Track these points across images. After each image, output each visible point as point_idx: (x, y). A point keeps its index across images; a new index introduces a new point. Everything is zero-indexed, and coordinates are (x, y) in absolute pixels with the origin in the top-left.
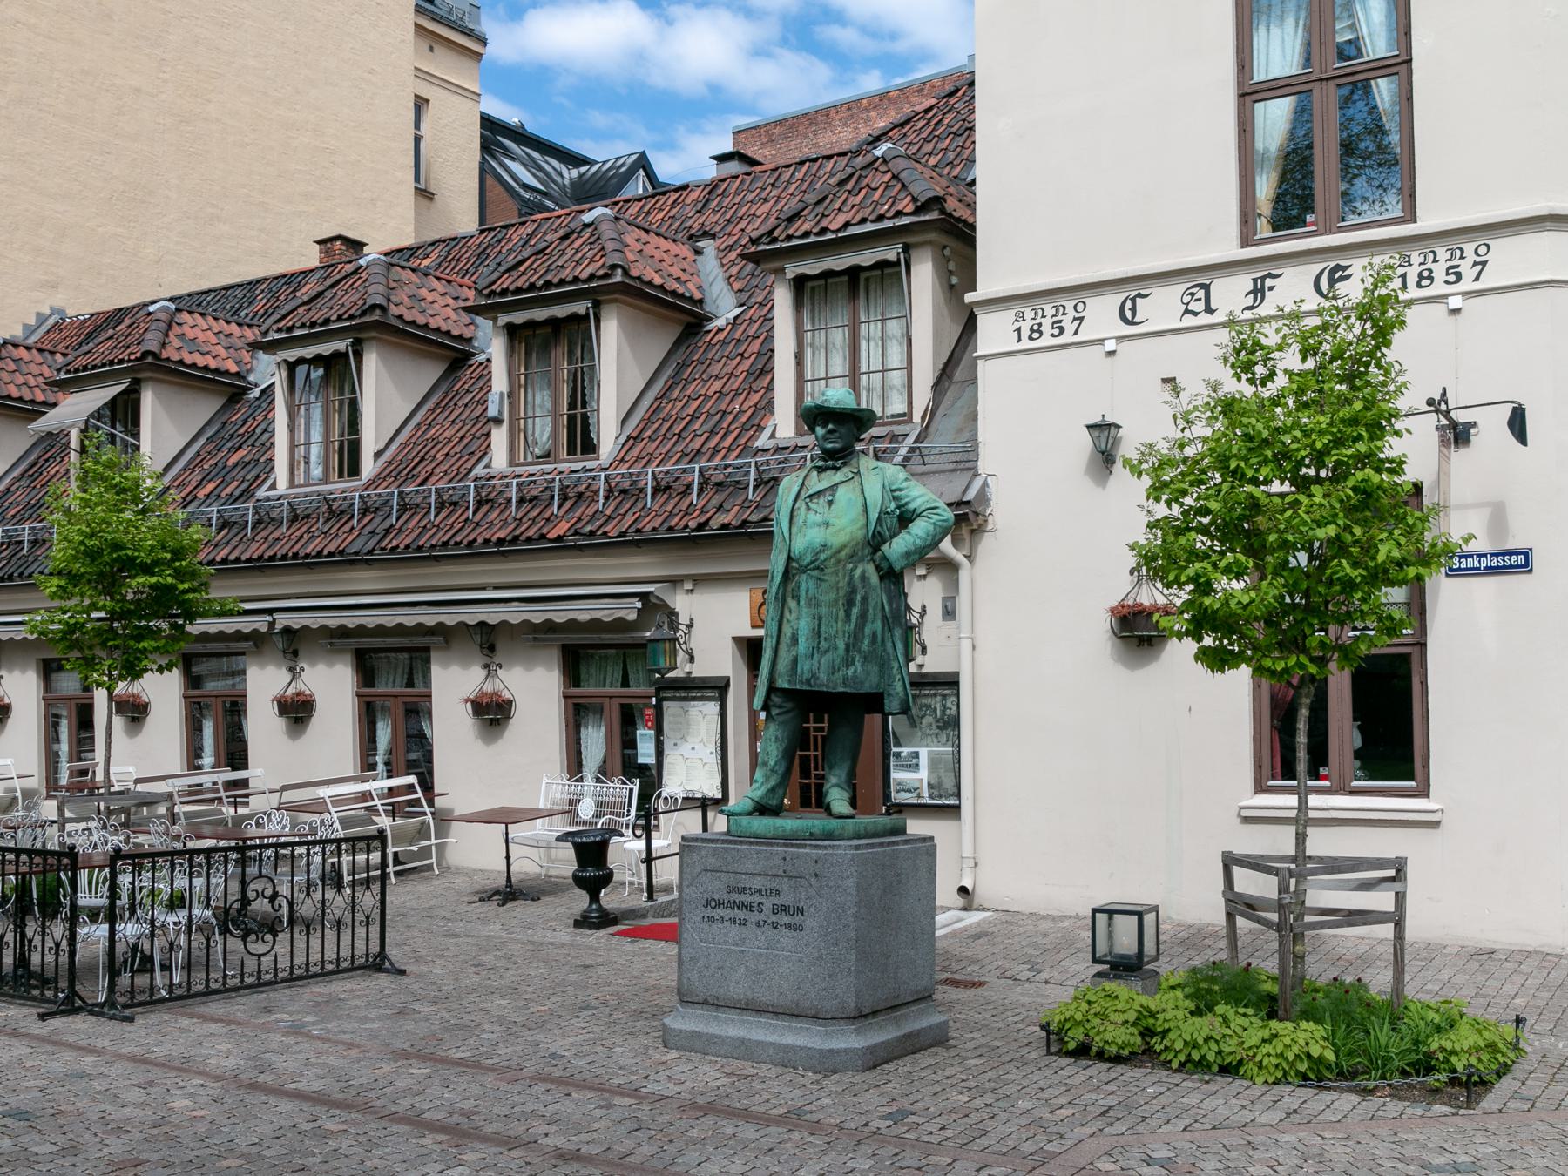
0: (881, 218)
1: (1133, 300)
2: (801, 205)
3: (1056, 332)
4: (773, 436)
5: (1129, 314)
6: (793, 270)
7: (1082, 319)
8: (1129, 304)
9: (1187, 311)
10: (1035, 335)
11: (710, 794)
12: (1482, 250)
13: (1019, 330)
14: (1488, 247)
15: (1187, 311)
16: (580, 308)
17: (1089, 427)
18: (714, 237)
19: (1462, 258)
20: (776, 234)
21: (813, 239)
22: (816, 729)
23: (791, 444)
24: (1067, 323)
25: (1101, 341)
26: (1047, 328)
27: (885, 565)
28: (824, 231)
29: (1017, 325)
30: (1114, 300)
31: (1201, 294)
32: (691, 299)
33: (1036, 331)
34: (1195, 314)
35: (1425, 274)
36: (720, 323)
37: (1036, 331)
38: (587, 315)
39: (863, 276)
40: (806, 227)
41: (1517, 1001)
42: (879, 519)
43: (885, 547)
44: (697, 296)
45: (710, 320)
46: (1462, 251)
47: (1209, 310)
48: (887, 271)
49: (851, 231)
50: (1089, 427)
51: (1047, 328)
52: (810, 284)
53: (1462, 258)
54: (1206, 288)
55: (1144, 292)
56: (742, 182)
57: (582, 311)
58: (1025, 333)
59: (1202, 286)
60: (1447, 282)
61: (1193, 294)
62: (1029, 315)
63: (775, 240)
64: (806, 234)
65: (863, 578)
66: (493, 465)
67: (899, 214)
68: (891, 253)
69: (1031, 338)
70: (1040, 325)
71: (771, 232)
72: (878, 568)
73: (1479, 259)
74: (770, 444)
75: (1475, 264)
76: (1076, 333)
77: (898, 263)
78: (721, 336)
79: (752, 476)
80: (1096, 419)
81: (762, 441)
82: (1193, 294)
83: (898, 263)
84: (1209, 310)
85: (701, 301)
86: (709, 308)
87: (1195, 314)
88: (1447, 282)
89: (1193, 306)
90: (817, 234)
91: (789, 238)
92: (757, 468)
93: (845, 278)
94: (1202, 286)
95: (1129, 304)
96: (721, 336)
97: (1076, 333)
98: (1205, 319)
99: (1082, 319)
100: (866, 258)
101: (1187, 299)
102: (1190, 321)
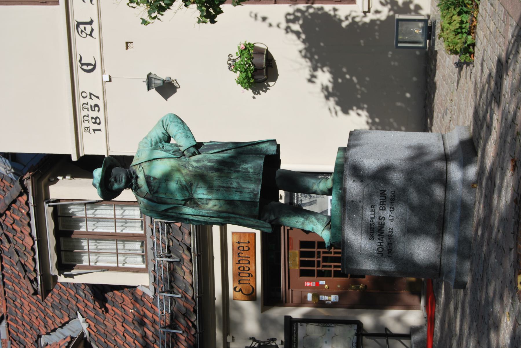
0: (29, 214)
1: (83, 64)
2: (19, 264)
3: (97, 109)
4: (148, 287)
5: (90, 67)
6: (53, 271)
7: (91, 94)
8: (85, 67)
9: (91, 35)
10: (98, 121)
11: (354, 332)
12: (84, 95)
13: (94, 130)
14: (83, 92)
15: (91, 35)
16: (48, 210)
17: (148, 90)
18: (39, 336)
19: (87, 104)
20: (32, 278)
21: (37, 257)
22: (319, 266)
23: (152, 274)
24: (92, 102)
25: (103, 83)
26: (94, 114)
27: (193, 150)
28: (33, 249)
29: (92, 131)
30: (81, 75)
31: (82, 27)
32: (70, 343)
33: (96, 120)
34: (92, 30)
35: (94, 121)
36: (85, 326)
37: (96, 120)
38: (53, 206)
39: (61, 228)
40: (30, 261)
41: (481, 18)
42: (166, 151)
43: (182, 149)
44: (69, 339)
45: (83, 334)
46: (84, 104)
47: (91, 23)
48: (59, 214)
49: (34, 233)
50: (148, 90)
51: (94, 114)
52: (63, 262)
53: (87, 104)
54: (79, 24)
55: (79, 59)
56: (12, 320)
57: (51, 209)
58: (96, 127)
59: (78, 26)
60: (99, 111)
61: (82, 31)
62: (86, 124)
63: (36, 279)
64: (34, 260)
65: (198, 161)
66: (148, 285)
67: (27, 203)
68: (48, 210)
69: (99, 124)
70: (92, 118)
71: (32, 282)
72: (194, 154)
73: (89, 96)
74: (152, 288)
75: (91, 98)
76: (98, 98)
77: (55, 207)
78: (92, 324)
79: (169, 295)
80: (145, 86)
81: (150, 293)
82: (82, 31)
83: (55, 207)
84: (91, 23)
85: (72, 338)
86: (76, 335)
87: (92, 30)
88: (99, 111)
89: (88, 31)
90: (35, 254)
91: (35, 270)
92: (164, 292)
93: (62, 239)
94: (78, 26)
95: (85, 67)
96: (92, 324)
97: (98, 98)
98: (95, 25)
99: (91, 94)
100: (50, 225)
101: (84, 35)
102: (95, 34)
